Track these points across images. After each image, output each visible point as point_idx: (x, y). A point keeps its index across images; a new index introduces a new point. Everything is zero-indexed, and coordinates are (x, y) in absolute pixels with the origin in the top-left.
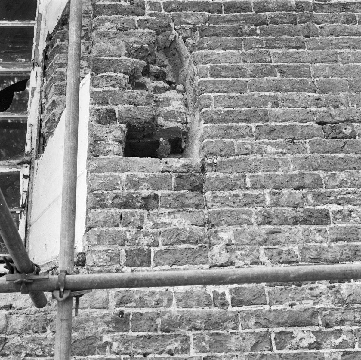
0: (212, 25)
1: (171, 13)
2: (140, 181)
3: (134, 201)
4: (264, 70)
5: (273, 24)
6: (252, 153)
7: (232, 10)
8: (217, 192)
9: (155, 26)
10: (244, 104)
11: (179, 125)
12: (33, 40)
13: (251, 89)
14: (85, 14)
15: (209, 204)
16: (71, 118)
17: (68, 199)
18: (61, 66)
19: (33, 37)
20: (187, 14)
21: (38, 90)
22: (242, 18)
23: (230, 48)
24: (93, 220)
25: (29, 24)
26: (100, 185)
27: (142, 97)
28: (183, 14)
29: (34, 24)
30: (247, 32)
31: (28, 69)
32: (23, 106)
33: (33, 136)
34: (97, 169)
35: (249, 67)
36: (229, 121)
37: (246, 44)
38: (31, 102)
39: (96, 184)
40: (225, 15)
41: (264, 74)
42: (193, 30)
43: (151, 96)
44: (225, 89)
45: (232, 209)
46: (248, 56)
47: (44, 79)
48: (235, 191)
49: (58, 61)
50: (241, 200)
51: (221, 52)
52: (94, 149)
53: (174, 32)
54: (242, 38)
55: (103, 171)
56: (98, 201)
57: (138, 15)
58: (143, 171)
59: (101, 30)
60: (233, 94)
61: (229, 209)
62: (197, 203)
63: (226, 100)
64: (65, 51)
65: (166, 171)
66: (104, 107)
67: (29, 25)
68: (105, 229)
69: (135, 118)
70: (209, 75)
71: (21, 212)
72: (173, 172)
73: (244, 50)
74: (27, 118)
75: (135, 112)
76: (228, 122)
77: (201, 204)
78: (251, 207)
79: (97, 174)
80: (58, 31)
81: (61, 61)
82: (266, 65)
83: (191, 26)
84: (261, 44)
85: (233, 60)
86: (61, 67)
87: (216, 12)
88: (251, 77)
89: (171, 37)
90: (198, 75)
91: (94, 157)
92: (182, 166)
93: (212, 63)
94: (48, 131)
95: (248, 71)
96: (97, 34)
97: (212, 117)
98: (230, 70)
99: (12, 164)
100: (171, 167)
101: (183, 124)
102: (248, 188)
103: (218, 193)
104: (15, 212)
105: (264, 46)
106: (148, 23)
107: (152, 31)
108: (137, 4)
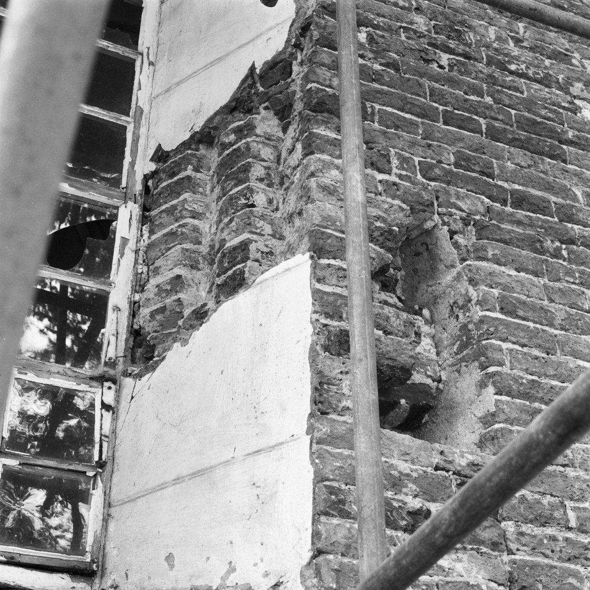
0: (494, 222)
1: (433, 184)
2: (403, 478)
3: (394, 514)
4: (579, 322)
5: (585, 246)
6: (573, 466)
7: (525, 205)
8: (522, 525)
9: (410, 198)
10: (556, 375)
11: (429, 381)
12: (123, 152)
13: (563, 351)
14: (266, 139)
15: (513, 546)
16: (368, 347)
17: (377, 505)
18: (195, 215)
19: (124, 145)
20: (458, 192)
21: (132, 245)
22: (540, 223)
23: (527, 271)
24: (326, 538)
25: (118, 119)
26: (336, 471)
27: (398, 322)
28: (452, 189)
29: (128, 122)
30: (550, 249)
31: (114, 202)
32: (102, 269)
33: (120, 331)
34: (329, 439)
35: (559, 311)
36: (535, 399)
37: (549, 269)
38: (119, 265)
39: (329, 468)
40: (511, 210)
41: (581, 330)
42: (466, 222)
43: (411, 323)
44: (525, 341)
45: (550, 562)
46: (556, 293)
47: (144, 227)
48: (550, 529)
49: (190, 206)
50: (563, 549)
51: (513, 273)
52: (322, 399)
53: (436, 217)
54: (544, 257)
55: (338, 445)
56: (334, 503)
57: (380, 171)
58: (406, 461)
59: (323, 179)
60: (536, 352)
61: (546, 561)
62: (495, 539)
63: (528, 360)
64: (201, 190)
65: (443, 469)
66: (336, 323)
67: (119, 122)
68: (346, 560)
69: (387, 356)
70: (498, 308)
71: (95, 476)
72: (454, 473)
73: (546, 280)
74: (109, 293)
75: (387, 346)
76: (534, 401)
77: (501, 544)
78: (580, 566)
79: (328, 448)
80: (189, 152)
81: (195, 206)
82: (582, 315)
83: (464, 215)
84: (572, 277)
85: (535, 291)
86: (194, 218)
87: (499, 202)
88: (562, 329)
89: (429, 225)
90: (479, 303)
91: (319, 413)
92: (468, 465)
93: (501, 289)
94: (158, 329)
95: (557, 319)
96: (319, 186)
97: (510, 386)
98: (531, 309)
99: (81, 376)
100: (451, 462)
101: (434, 381)
102: (570, 529)
103: (525, 528)
104: (85, 473)
105: (577, 281)
106: (398, 190)
107: (404, 206)
108: (379, 151)
